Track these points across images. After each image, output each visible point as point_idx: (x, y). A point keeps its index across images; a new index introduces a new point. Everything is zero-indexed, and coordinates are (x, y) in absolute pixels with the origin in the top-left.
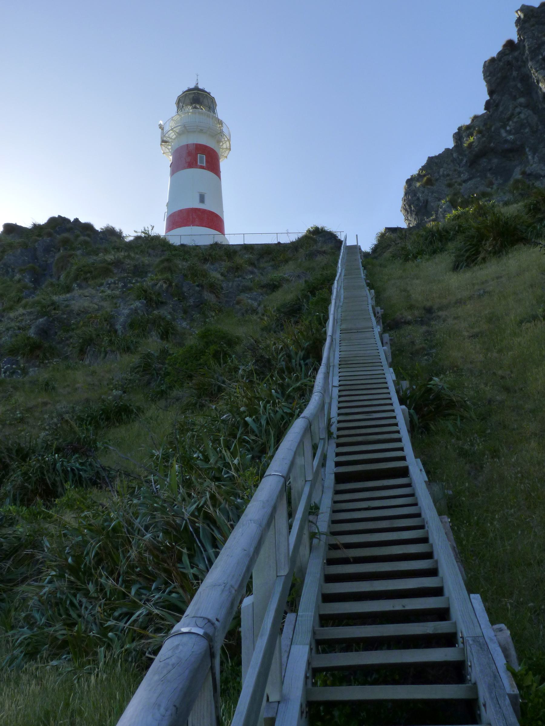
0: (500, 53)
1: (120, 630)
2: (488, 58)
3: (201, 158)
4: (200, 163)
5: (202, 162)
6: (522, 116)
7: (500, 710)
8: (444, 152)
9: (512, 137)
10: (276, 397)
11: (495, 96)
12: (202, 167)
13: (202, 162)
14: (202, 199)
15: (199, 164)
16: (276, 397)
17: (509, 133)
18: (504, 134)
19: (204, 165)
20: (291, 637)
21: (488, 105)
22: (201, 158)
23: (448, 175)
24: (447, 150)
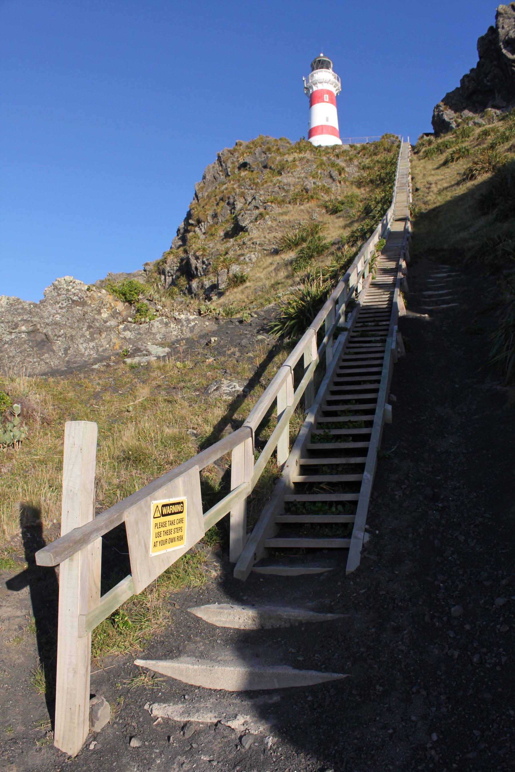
0: (486, 35)
1: (67, 757)
2: (480, 36)
3: (326, 97)
5: (326, 99)
6: (495, 72)
7: (122, 336)
8: (455, 90)
9: (489, 83)
10: (419, 139)
11: (482, 60)
12: (327, 102)
13: (326, 99)
14: (327, 120)
16: (419, 139)
17: (488, 81)
18: (485, 81)
20: (258, 362)
21: (478, 64)
22: (326, 97)
23: (456, 104)
24: (457, 88)
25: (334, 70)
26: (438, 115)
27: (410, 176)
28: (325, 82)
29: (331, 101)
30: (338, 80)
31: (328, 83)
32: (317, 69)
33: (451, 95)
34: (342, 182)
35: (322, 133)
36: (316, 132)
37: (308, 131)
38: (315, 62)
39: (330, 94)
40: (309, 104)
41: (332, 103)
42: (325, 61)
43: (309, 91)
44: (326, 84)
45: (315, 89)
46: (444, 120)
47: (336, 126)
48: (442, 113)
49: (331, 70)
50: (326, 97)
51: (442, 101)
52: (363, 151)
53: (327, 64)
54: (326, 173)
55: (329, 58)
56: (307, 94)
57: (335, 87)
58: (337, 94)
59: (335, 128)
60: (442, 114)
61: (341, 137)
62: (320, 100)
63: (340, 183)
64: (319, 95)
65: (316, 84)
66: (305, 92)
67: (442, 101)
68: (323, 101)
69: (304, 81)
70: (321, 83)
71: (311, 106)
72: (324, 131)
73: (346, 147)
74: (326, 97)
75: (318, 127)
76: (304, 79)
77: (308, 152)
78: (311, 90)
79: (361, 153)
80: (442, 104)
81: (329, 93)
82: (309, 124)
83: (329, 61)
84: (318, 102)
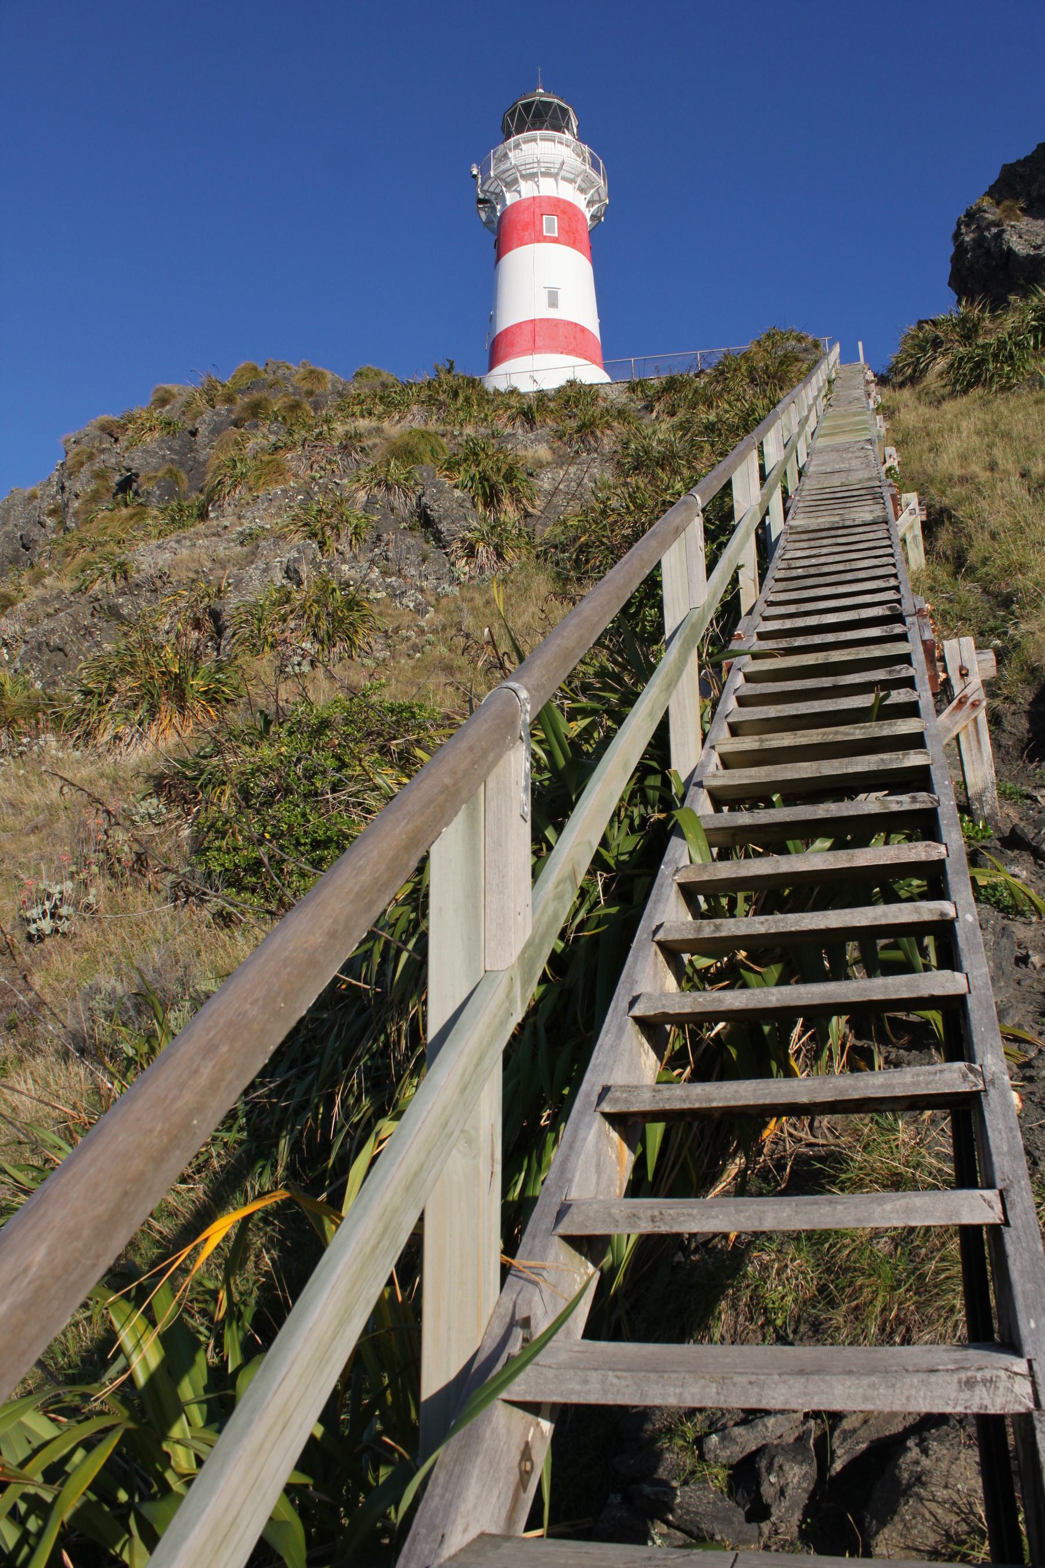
3: (549, 221)
4: (548, 231)
5: (550, 229)
12: (555, 240)
14: (553, 300)
15: (545, 234)
19: (556, 235)
25: (582, 138)
26: (979, 241)
27: (911, 498)
28: (545, 174)
29: (568, 237)
30: (595, 166)
31: (555, 176)
32: (519, 131)
33: (1020, 170)
34: (480, 547)
35: (533, 349)
36: (513, 345)
37: (487, 346)
38: (512, 115)
39: (564, 212)
40: (494, 252)
41: (573, 244)
42: (551, 103)
43: (494, 209)
44: (552, 180)
45: (510, 198)
46: (1010, 250)
47: (591, 323)
48: (994, 230)
49: (567, 136)
50: (551, 225)
51: (989, 194)
52: (666, 398)
53: (554, 117)
54: (398, 500)
55: (561, 99)
56: (489, 221)
57: (582, 190)
58: (593, 217)
59: (583, 330)
60: (999, 235)
61: (607, 368)
62: (526, 235)
63: (471, 552)
64: (526, 217)
65: (515, 181)
66: (483, 216)
67: (989, 194)
68: (540, 238)
69: (475, 176)
70: (531, 177)
71: (499, 257)
72: (539, 342)
73: (618, 395)
74: (551, 225)
75: (519, 325)
76: (475, 172)
77: (415, 408)
78: (499, 207)
79: (658, 407)
80: (987, 203)
81: (562, 208)
82: (492, 319)
83: (566, 106)
84: (522, 243)
